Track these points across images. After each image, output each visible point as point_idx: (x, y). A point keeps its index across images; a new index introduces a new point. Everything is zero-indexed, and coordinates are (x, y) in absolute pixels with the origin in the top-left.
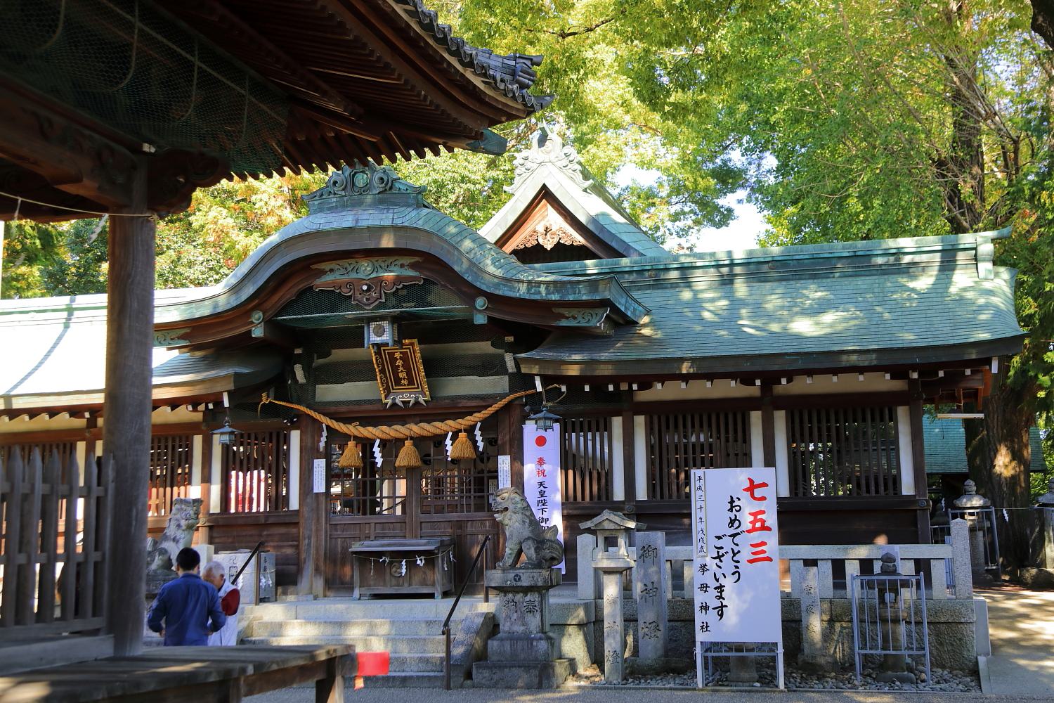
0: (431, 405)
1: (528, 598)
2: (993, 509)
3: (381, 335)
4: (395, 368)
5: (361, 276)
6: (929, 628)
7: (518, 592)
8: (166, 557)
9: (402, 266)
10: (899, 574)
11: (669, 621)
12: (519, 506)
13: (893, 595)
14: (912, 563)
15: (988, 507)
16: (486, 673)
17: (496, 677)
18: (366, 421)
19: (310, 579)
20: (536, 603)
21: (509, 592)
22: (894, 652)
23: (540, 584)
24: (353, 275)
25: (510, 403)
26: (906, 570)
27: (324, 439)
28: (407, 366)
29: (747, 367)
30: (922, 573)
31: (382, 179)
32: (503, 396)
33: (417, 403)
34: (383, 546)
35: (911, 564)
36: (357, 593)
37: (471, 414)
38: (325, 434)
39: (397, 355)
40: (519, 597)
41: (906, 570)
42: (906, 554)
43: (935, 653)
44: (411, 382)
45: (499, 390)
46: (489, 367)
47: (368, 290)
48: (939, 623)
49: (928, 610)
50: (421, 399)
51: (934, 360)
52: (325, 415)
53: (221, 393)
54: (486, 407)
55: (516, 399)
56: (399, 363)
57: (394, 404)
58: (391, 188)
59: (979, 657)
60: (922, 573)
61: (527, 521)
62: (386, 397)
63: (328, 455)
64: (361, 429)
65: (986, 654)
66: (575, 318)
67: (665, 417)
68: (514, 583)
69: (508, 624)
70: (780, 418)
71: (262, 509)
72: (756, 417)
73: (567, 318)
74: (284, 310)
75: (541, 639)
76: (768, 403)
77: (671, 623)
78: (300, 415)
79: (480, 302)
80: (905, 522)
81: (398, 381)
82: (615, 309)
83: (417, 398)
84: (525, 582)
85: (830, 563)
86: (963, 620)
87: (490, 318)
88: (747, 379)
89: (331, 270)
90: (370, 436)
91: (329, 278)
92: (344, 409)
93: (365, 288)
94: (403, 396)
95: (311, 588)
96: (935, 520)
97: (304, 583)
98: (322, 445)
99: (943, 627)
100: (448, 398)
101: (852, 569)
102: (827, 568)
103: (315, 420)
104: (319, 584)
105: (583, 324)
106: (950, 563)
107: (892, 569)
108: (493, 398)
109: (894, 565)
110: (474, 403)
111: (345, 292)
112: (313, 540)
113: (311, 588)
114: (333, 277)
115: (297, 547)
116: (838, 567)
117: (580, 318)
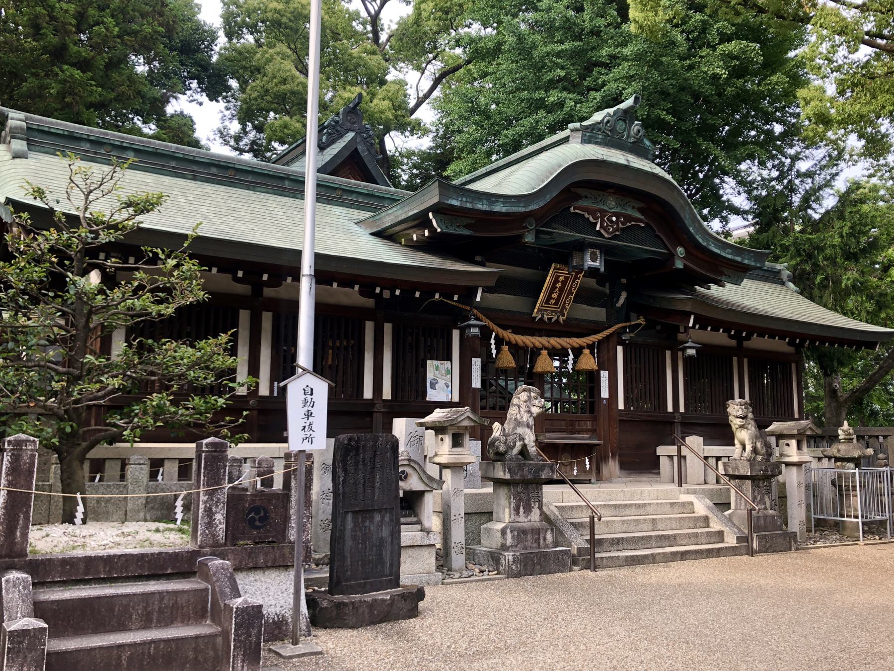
9: (633, 208)
33: (557, 321)
56: (559, 285)
76: (740, 351)
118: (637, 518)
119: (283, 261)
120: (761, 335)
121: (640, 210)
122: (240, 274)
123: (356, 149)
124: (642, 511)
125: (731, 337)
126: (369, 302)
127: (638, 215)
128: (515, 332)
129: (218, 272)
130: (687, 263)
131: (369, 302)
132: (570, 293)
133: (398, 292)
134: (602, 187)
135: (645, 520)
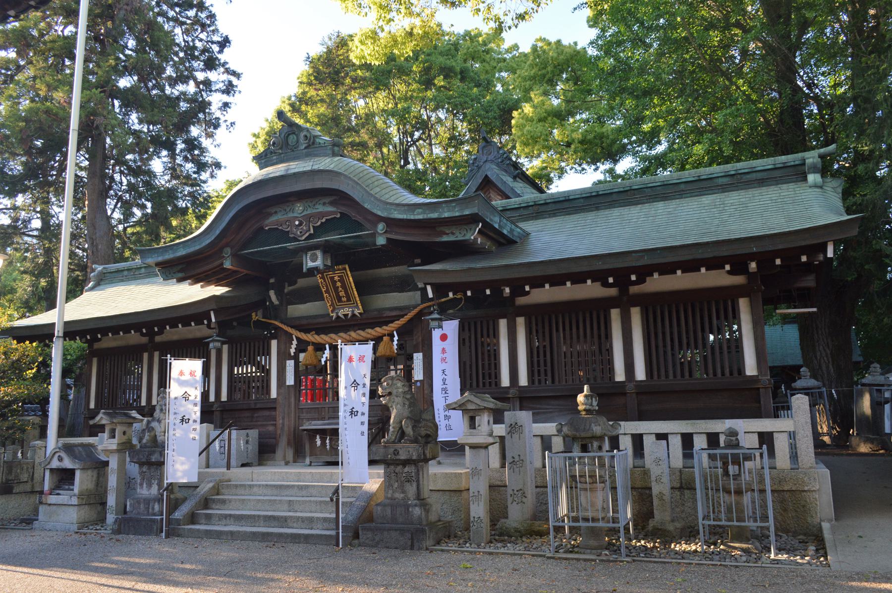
0: (364, 316)
1: (406, 469)
2: (824, 389)
3: (314, 261)
4: (336, 289)
5: (295, 215)
6: (773, 495)
7: (398, 465)
8: (152, 434)
9: (324, 204)
10: (742, 448)
11: (537, 487)
12: (400, 390)
13: (737, 467)
14: (756, 436)
15: (819, 388)
16: (370, 535)
17: (377, 538)
18: (320, 331)
19: (284, 449)
20: (413, 474)
21: (391, 464)
22: (738, 524)
23: (414, 458)
24: (291, 215)
25: (421, 311)
26: (749, 442)
27: (294, 346)
28: (344, 286)
29: (599, 266)
30: (765, 447)
31: (306, 136)
32: (415, 307)
33: (354, 315)
34: (328, 424)
35: (755, 437)
36: (308, 461)
37: (392, 322)
38: (295, 342)
39: (336, 278)
40: (399, 469)
41: (749, 442)
42: (748, 429)
43: (780, 518)
44: (349, 300)
45: (413, 303)
46: (404, 284)
47: (300, 224)
48: (784, 491)
49: (772, 479)
50: (357, 312)
51: (771, 248)
52: (292, 327)
53: (209, 312)
54: (403, 316)
55: (425, 308)
56: (339, 284)
57: (338, 317)
58: (313, 143)
59: (823, 524)
60: (765, 447)
61: (407, 403)
62: (332, 312)
63: (296, 358)
64: (316, 336)
65: (830, 521)
66: (453, 234)
67: (542, 319)
68: (394, 457)
69: (390, 492)
70: (636, 314)
71: (224, 397)
72: (615, 314)
73: (447, 234)
74: (245, 246)
75: (416, 505)
76: (624, 302)
77: (538, 489)
78: (277, 328)
79: (381, 227)
80: (750, 399)
81: (339, 299)
82: (487, 225)
83: (353, 311)
84: (403, 456)
85: (679, 437)
86: (806, 488)
87: (388, 239)
88: (599, 277)
89: (276, 212)
90: (323, 342)
91: (274, 218)
92: (304, 322)
93: (297, 223)
94: (345, 311)
95: (285, 456)
96: (777, 400)
97: (279, 453)
98: (292, 351)
99: (787, 495)
100: (376, 310)
101: (700, 442)
102: (676, 442)
103: (286, 332)
104: (290, 454)
105: (460, 238)
106: (792, 435)
107: (735, 442)
108: (408, 308)
109: (737, 439)
110: (394, 313)
111: (285, 228)
112: (284, 422)
113: (285, 456)
114: (276, 219)
115: (275, 425)
116: (687, 440)
117: (457, 234)
118: (273, 498)
119: (46, 332)
120: (174, 325)
121: (332, 203)
122: (611, 280)
123: (486, 176)
124: (304, 493)
125: (143, 335)
126: (739, 280)
127: (330, 209)
128: (318, 334)
129: (550, 286)
130: (389, 236)
131: (739, 280)
132: (327, 291)
133: (469, 293)
134: (284, 200)
135: (280, 501)
